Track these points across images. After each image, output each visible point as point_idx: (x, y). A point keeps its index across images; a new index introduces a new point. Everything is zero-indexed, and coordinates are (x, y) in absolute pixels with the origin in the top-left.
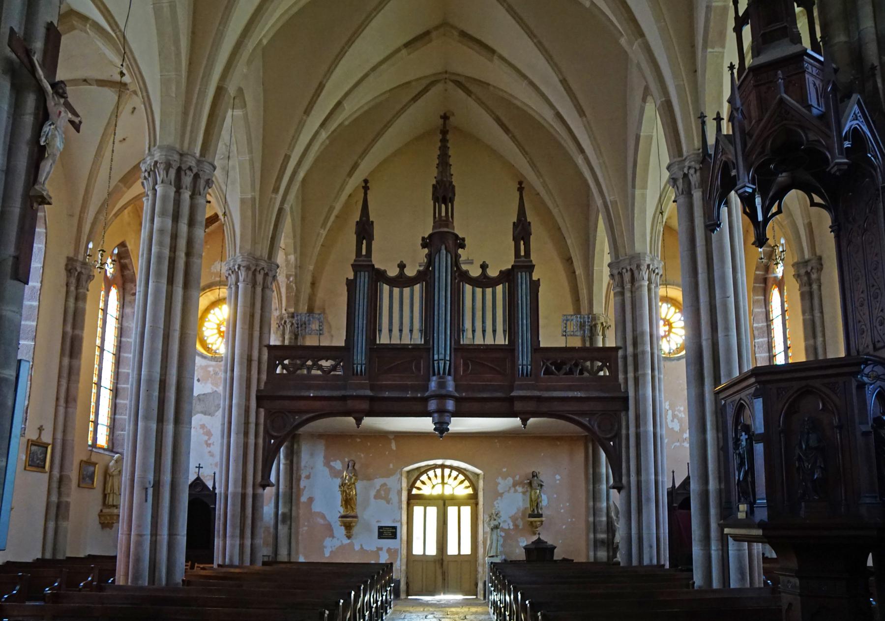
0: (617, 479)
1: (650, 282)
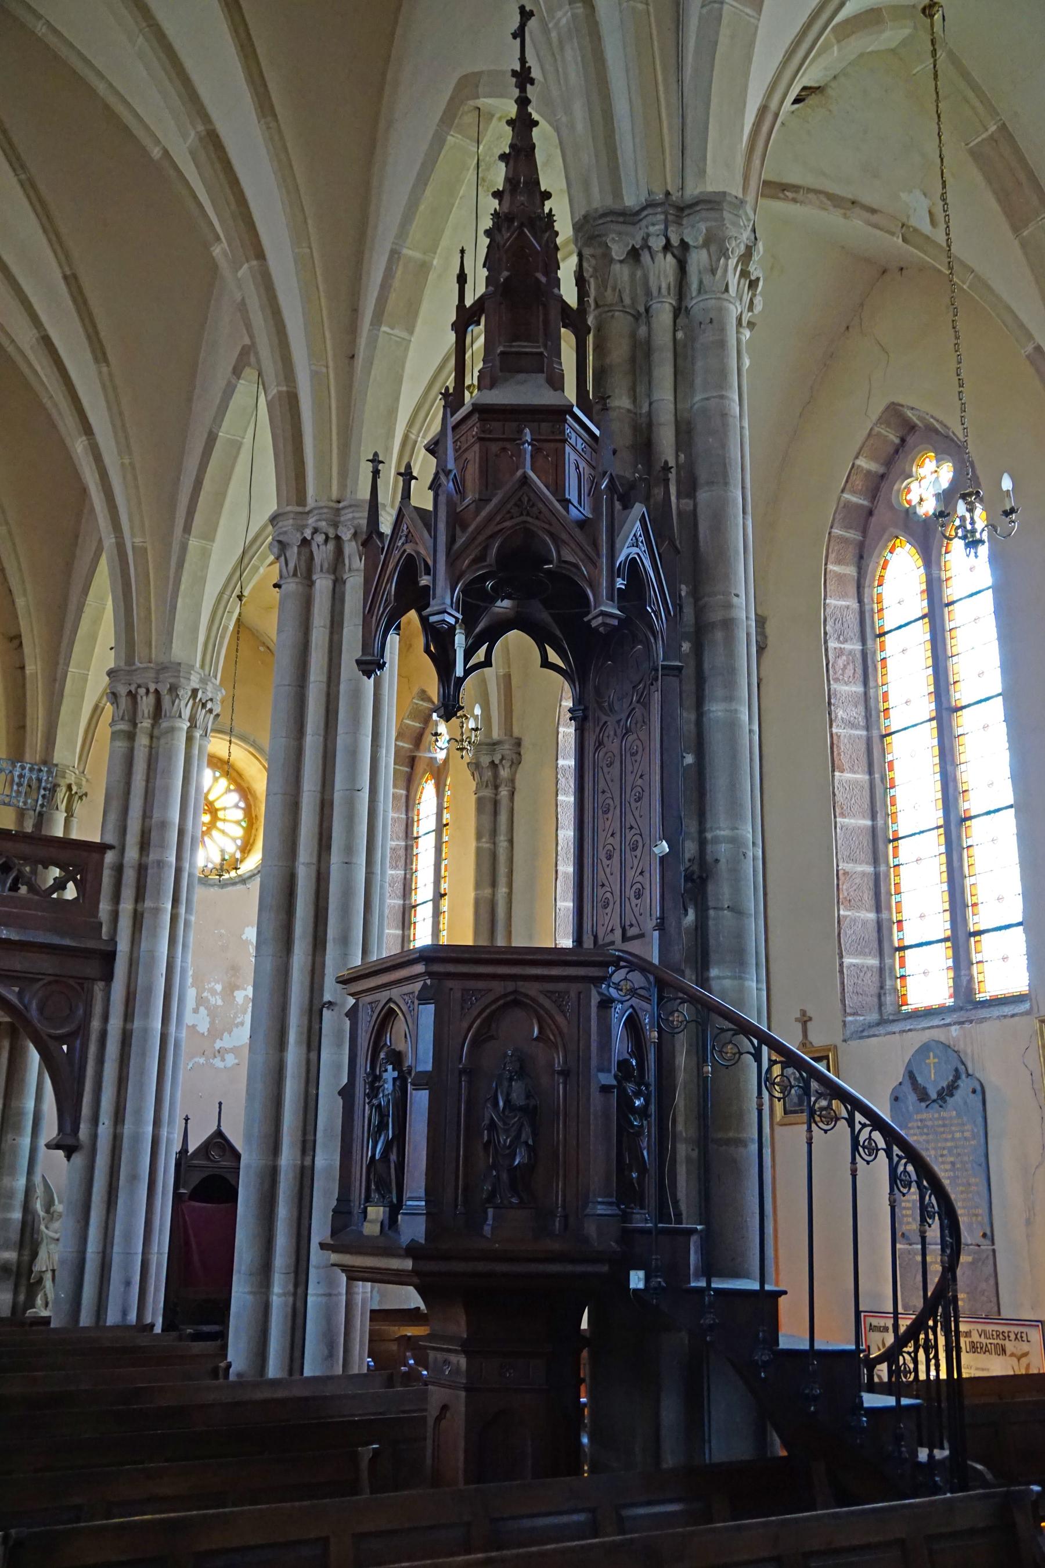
0: (68, 1129)
1: (193, 726)
